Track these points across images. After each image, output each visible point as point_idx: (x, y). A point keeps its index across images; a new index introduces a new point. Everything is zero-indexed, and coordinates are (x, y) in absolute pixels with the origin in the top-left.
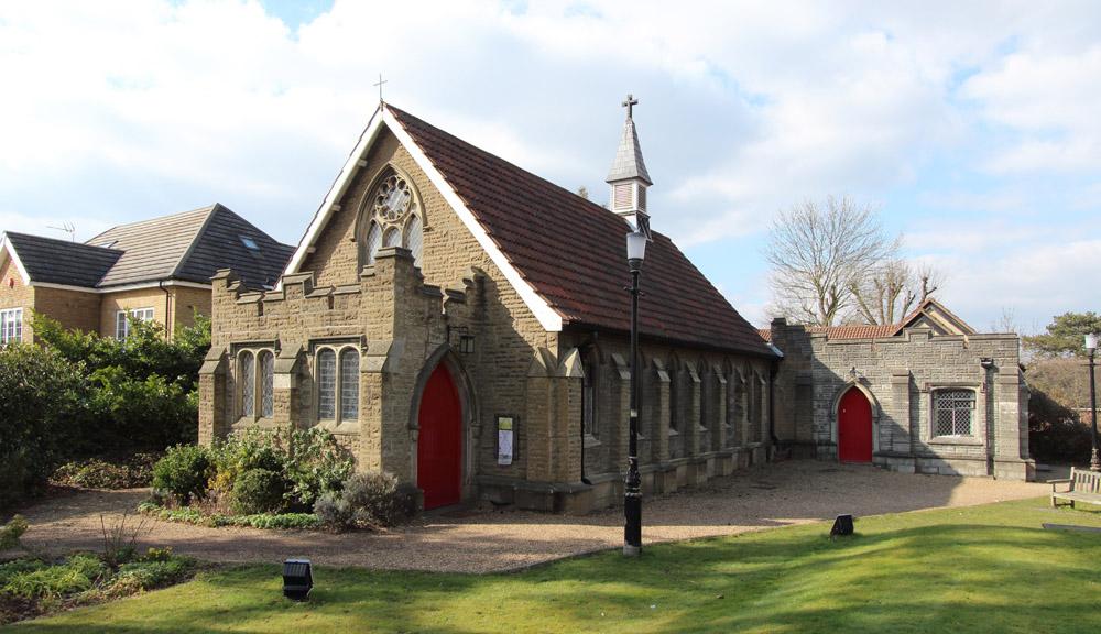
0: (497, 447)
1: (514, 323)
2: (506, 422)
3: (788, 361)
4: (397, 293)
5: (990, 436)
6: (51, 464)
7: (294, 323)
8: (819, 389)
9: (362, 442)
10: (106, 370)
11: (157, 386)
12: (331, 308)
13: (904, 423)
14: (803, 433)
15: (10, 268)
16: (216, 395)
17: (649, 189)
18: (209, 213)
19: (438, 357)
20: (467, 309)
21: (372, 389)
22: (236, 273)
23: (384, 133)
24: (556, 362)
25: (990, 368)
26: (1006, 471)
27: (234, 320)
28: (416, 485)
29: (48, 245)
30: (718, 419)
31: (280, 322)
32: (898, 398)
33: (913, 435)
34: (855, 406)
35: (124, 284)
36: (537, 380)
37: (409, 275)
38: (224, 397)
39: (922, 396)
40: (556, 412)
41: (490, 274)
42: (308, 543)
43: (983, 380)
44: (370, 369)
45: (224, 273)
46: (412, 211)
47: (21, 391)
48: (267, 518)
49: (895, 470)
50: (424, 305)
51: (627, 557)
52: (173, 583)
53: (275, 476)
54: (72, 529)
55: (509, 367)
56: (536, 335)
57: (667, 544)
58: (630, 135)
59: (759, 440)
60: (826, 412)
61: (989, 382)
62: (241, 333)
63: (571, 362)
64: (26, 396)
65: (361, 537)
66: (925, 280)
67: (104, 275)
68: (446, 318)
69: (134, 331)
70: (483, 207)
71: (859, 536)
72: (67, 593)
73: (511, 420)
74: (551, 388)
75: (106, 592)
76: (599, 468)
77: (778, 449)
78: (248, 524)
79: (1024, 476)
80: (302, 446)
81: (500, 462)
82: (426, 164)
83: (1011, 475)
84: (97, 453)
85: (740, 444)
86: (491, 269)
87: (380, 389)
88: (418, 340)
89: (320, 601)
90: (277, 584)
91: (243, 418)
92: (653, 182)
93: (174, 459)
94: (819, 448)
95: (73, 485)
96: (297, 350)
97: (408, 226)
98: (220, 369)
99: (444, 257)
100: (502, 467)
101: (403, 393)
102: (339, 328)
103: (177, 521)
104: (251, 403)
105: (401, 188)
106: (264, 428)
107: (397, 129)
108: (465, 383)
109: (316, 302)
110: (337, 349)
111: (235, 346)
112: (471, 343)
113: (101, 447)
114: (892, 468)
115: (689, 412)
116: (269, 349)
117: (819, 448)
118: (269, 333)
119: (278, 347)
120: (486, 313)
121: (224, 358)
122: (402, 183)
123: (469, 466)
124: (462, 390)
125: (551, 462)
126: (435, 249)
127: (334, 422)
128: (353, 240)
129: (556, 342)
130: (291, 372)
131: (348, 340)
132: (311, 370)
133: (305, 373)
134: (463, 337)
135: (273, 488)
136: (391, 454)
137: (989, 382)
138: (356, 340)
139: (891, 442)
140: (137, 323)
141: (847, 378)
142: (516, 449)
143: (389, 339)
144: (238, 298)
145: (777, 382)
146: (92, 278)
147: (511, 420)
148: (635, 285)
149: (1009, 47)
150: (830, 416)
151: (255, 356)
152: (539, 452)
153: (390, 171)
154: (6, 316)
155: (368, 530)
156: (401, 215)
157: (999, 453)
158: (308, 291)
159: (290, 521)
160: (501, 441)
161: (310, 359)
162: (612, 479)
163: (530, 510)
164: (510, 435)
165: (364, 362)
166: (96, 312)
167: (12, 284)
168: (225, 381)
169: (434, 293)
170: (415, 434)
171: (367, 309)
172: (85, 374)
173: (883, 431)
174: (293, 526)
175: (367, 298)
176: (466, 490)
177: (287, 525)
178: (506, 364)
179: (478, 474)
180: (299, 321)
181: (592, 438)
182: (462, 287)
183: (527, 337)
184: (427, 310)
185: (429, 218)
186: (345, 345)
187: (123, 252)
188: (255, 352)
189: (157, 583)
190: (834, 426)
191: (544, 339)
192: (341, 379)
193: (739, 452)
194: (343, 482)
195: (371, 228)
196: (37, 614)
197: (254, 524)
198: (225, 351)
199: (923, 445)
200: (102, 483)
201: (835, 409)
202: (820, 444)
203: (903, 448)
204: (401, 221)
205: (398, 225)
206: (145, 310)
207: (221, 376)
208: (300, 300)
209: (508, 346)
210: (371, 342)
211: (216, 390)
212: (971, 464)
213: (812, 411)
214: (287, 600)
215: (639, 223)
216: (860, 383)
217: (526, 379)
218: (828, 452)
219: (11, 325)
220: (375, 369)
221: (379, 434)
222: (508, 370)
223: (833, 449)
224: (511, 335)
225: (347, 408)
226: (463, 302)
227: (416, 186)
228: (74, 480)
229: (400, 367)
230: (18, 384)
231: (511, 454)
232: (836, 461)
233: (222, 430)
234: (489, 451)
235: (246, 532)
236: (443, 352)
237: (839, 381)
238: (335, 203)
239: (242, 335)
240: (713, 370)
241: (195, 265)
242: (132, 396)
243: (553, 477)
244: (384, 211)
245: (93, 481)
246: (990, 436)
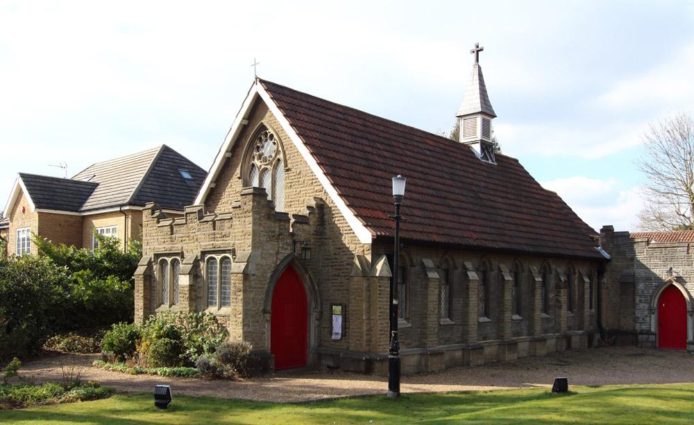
0: (331, 327)
1: (343, 238)
2: (337, 309)
3: (614, 263)
4: (254, 219)
6: (43, 336)
7: (193, 239)
8: (641, 286)
9: (231, 320)
10: (80, 273)
11: (114, 283)
12: (214, 229)
14: (626, 324)
15: (22, 199)
16: (145, 289)
17: (493, 121)
18: (157, 153)
19: (285, 263)
20: (310, 228)
22: (158, 205)
23: (258, 100)
24: (370, 267)
27: (156, 238)
28: (270, 352)
29: (45, 181)
30: (533, 310)
31: (184, 239)
35: (104, 208)
36: (356, 279)
37: (263, 206)
38: (151, 290)
40: (369, 302)
41: (327, 202)
42: (184, 384)
44: (236, 271)
45: (150, 205)
46: (278, 157)
47: (24, 287)
48: (168, 370)
50: (276, 227)
51: (389, 399)
52: (98, 398)
53: (176, 343)
54: (50, 373)
55: (340, 269)
56: (358, 246)
57: (427, 393)
58: (476, 77)
59: (582, 329)
60: (646, 306)
62: (160, 247)
63: (380, 265)
64: (28, 291)
65: (224, 383)
67: (84, 203)
68: (292, 235)
69: (99, 243)
70: (324, 152)
71: (571, 394)
72: (39, 400)
73: (340, 307)
74: (365, 285)
75: (60, 400)
76: (409, 344)
77: (602, 337)
78: (156, 373)
80: (194, 324)
81: (334, 337)
82: (284, 123)
84: (74, 330)
85: (558, 331)
86: (328, 199)
88: (271, 251)
89: (175, 409)
90: (153, 402)
91: (162, 305)
92: (496, 113)
93: (117, 332)
94: (640, 337)
95: (59, 350)
96: (148, 260)
97: (276, 167)
98: (148, 271)
99: (298, 190)
100: (335, 341)
101: (260, 288)
102: (219, 243)
103: (113, 370)
104: (167, 295)
105: (271, 140)
106: (173, 312)
107: (266, 97)
108: (308, 280)
109: (206, 226)
110: (218, 257)
111: (157, 256)
112: (308, 253)
113: (77, 325)
115: (501, 303)
116: (177, 258)
117: (640, 337)
118: (177, 247)
119: (183, 257)
120: (325, 230)
121: (150, 264)
122: (272, 136)
123: (312, 340)
124: (307, 285)
125: (365, 338)
126: (292, 184)
127: (217, 308)
128: (239, 178)
129: (370, 251)
130: (189, 274)
131: (224, 251)
132: (202, 272)
133: (199, 274)
134: (303, 249)
135: (174, 350)
136: (249, 330)
140: (101, 239)
142: (344, 328)
143: (249, 250)
144: (158, 222)
145: (605, 280)
146: (75, 204)
147: (340, 307)
148: (398, 213)
150: (651, 310)
151: (169, 263)
153: (263, 127)
154: (20, 233)
155: (230, 378)
156: (271, 159)
159: (182, 372)
160: (334, 322)
162: (420, 352)
163: (351, 371)
164: (340, 319)
166: (78, 231)
167: (24, 211)
168: (151, 279)
169: (283, 217)
170: (268, 316)
172: (68, 274)
174: (183, 375)
175: (235, 222)
176: (311, 357)
177: (179, 375)
179: (319, 346)
180: (195, 238)
181: (405, 322)
182: (306, 212)
183: (352, 247)
184: (278, 230)
185: (289, 162)
186: (223, 255)
187: (98, 184)
188: (169, 260)
189: (89, 397)
191: (362, 249)
192: (221, 278)
193: (557, 338)
194: (216, 348)
195: (252, 169)
196: (23, 407)
197: (159, 373)
198: (151, 259)
200: (76, 349)
202: (642, 333)
205: (269, 167)
206: (111, 228)
207: (148, 276)
209: (339, 253)
210: (238, 252)
211: (144, 285)
213: (634, 306)
214: (155, 408)
215: (483, 149)
216: (676, 281)
217: (349, 278)
218: (647, 340)
219: (23, 240)
222: (339, 272)
224: (341, 246)
225: (225, 298)
226: (306, 223)
227: (279, 138)
228: (59, 347)
229: (257, 270)
230: (23, 281)
231: (340, 332)
232: (655, 348)
233: (149, 310)
234: (326, 330)
235: (154, 378)
236: (290, 258)
237: (658, 279)
238: (227, 151)
239: (161, 248)
240: (530, 271)
241: (145, 194)
242: (97, 290)
243: (367, 348)
244: (260, 157)
245: (70, 348)
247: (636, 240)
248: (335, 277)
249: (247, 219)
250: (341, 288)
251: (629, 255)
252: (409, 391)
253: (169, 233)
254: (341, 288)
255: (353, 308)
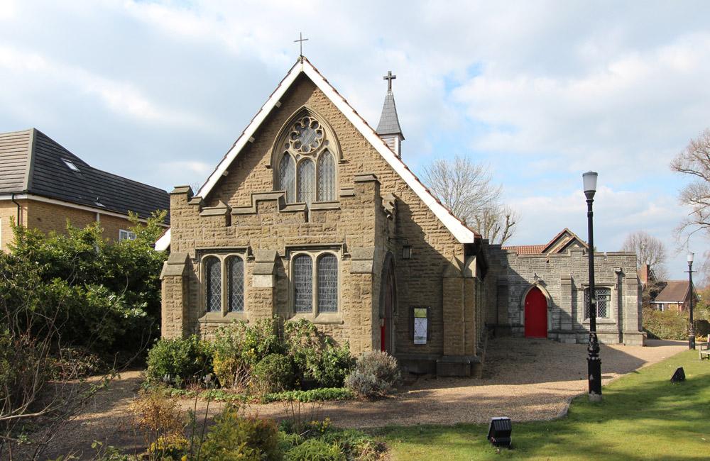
1: (426, 238)
2: (421, 312)
5: (620, 318)
8: (512, 289)
13: (569, 311)
21: (362, 287)
25: (620, 274)
26: (631, 340)
32: (565, 294)
33: (574, 319)
34: (536, 301)
36: (452, 280)
39: (579, 292)
43: (616, 282)
49: (564, 342)
55: (423, 270)
56: (445, 246)
60: (517, 304)
61: (620, 283)
66: (508, 217)
73: (425, 310)
79: (641, 342)
83: (634, 342)
87: (370, 286)
94: (513, 329)
96: (185, 257)
100: (417, 346)
102: (319, 238)
111: (200, 252)
114: (562, 341)
120: (400, 229)
122: (315, 123)
128: (268, 167)
129: (463, 252)
130: (272, 274)
137: (620, 283)
138: (242, 250)
139: (560, 323)
141: (532, 281)
144: (201, 210)
147: (425, 310)
149: (474, 71)
150: (520, 307)
152: (454, 333)
153: (305, 112)
157: (626, 328)
158: (283, 206)
161: (285, 263)
164: (425, 322)
165: (343, 267)
171: (346, 222)
173: (554, 317)
175: (346, 213)
178: (419, 268)
185: (344, 153)
190: (522, 313)
191: (452, 249)
199: (579, 325)
201: (523, 302)
202: (514, 326)
203: (567, 326)
204: (314, 154)
205: (311, 157)
208: (275, 214)
209: (420, 253)
212: (608, 336)
218: (519, 332)
220: (365, 270)
221: (370, 322)
222: (421, 272)
223: (523, 329)
224: (423, 246)
231: (425, 336)
237: (526, 283)
244: (297, 146)
246: (620, 318)
247: (508, 252)
248: (415, 279)
249: (366, 211)
250: (424, 290)
251: (502, 263)
252: (620, 386)
253: (224, 224)
254: (424, 290)
255: (447, 311)
